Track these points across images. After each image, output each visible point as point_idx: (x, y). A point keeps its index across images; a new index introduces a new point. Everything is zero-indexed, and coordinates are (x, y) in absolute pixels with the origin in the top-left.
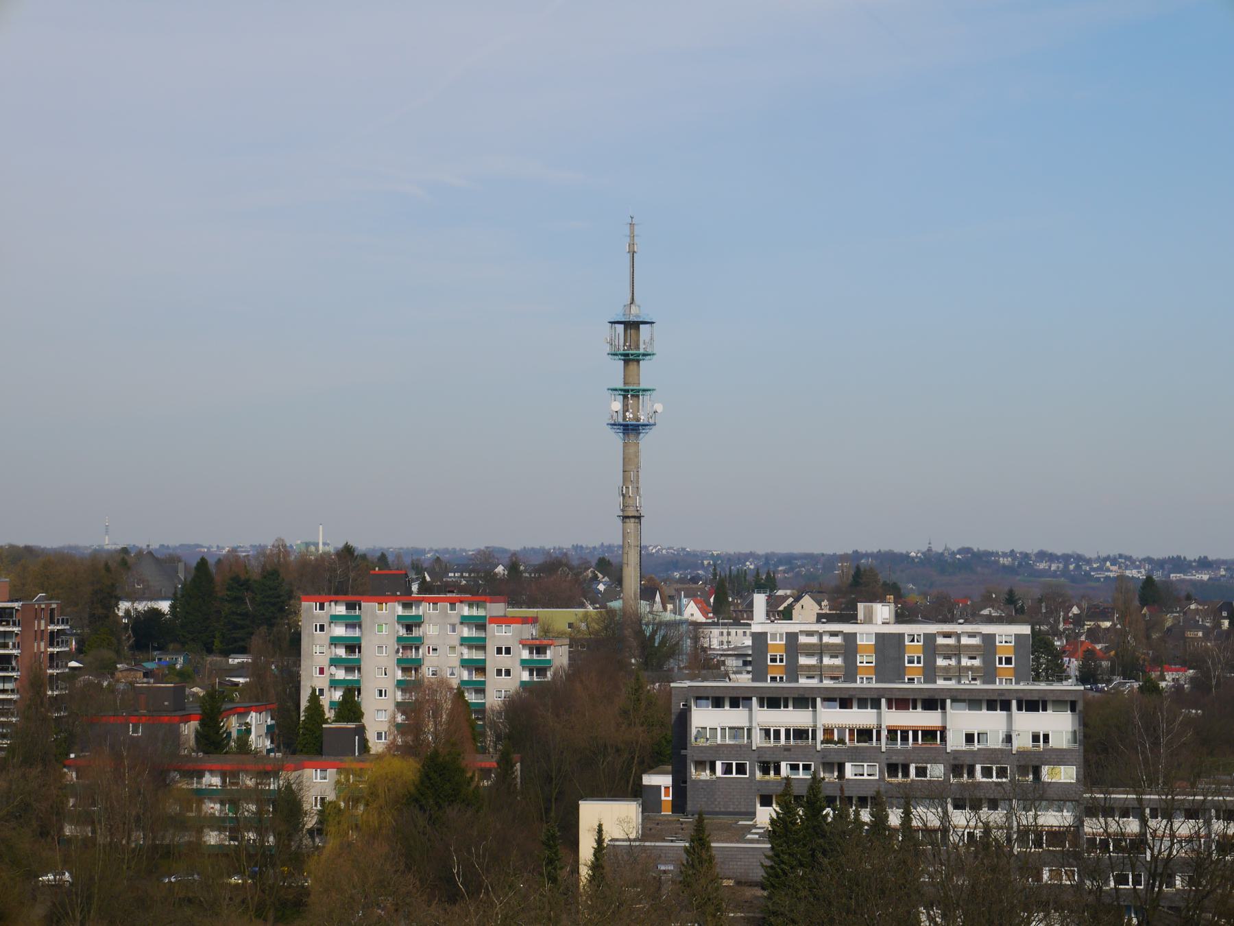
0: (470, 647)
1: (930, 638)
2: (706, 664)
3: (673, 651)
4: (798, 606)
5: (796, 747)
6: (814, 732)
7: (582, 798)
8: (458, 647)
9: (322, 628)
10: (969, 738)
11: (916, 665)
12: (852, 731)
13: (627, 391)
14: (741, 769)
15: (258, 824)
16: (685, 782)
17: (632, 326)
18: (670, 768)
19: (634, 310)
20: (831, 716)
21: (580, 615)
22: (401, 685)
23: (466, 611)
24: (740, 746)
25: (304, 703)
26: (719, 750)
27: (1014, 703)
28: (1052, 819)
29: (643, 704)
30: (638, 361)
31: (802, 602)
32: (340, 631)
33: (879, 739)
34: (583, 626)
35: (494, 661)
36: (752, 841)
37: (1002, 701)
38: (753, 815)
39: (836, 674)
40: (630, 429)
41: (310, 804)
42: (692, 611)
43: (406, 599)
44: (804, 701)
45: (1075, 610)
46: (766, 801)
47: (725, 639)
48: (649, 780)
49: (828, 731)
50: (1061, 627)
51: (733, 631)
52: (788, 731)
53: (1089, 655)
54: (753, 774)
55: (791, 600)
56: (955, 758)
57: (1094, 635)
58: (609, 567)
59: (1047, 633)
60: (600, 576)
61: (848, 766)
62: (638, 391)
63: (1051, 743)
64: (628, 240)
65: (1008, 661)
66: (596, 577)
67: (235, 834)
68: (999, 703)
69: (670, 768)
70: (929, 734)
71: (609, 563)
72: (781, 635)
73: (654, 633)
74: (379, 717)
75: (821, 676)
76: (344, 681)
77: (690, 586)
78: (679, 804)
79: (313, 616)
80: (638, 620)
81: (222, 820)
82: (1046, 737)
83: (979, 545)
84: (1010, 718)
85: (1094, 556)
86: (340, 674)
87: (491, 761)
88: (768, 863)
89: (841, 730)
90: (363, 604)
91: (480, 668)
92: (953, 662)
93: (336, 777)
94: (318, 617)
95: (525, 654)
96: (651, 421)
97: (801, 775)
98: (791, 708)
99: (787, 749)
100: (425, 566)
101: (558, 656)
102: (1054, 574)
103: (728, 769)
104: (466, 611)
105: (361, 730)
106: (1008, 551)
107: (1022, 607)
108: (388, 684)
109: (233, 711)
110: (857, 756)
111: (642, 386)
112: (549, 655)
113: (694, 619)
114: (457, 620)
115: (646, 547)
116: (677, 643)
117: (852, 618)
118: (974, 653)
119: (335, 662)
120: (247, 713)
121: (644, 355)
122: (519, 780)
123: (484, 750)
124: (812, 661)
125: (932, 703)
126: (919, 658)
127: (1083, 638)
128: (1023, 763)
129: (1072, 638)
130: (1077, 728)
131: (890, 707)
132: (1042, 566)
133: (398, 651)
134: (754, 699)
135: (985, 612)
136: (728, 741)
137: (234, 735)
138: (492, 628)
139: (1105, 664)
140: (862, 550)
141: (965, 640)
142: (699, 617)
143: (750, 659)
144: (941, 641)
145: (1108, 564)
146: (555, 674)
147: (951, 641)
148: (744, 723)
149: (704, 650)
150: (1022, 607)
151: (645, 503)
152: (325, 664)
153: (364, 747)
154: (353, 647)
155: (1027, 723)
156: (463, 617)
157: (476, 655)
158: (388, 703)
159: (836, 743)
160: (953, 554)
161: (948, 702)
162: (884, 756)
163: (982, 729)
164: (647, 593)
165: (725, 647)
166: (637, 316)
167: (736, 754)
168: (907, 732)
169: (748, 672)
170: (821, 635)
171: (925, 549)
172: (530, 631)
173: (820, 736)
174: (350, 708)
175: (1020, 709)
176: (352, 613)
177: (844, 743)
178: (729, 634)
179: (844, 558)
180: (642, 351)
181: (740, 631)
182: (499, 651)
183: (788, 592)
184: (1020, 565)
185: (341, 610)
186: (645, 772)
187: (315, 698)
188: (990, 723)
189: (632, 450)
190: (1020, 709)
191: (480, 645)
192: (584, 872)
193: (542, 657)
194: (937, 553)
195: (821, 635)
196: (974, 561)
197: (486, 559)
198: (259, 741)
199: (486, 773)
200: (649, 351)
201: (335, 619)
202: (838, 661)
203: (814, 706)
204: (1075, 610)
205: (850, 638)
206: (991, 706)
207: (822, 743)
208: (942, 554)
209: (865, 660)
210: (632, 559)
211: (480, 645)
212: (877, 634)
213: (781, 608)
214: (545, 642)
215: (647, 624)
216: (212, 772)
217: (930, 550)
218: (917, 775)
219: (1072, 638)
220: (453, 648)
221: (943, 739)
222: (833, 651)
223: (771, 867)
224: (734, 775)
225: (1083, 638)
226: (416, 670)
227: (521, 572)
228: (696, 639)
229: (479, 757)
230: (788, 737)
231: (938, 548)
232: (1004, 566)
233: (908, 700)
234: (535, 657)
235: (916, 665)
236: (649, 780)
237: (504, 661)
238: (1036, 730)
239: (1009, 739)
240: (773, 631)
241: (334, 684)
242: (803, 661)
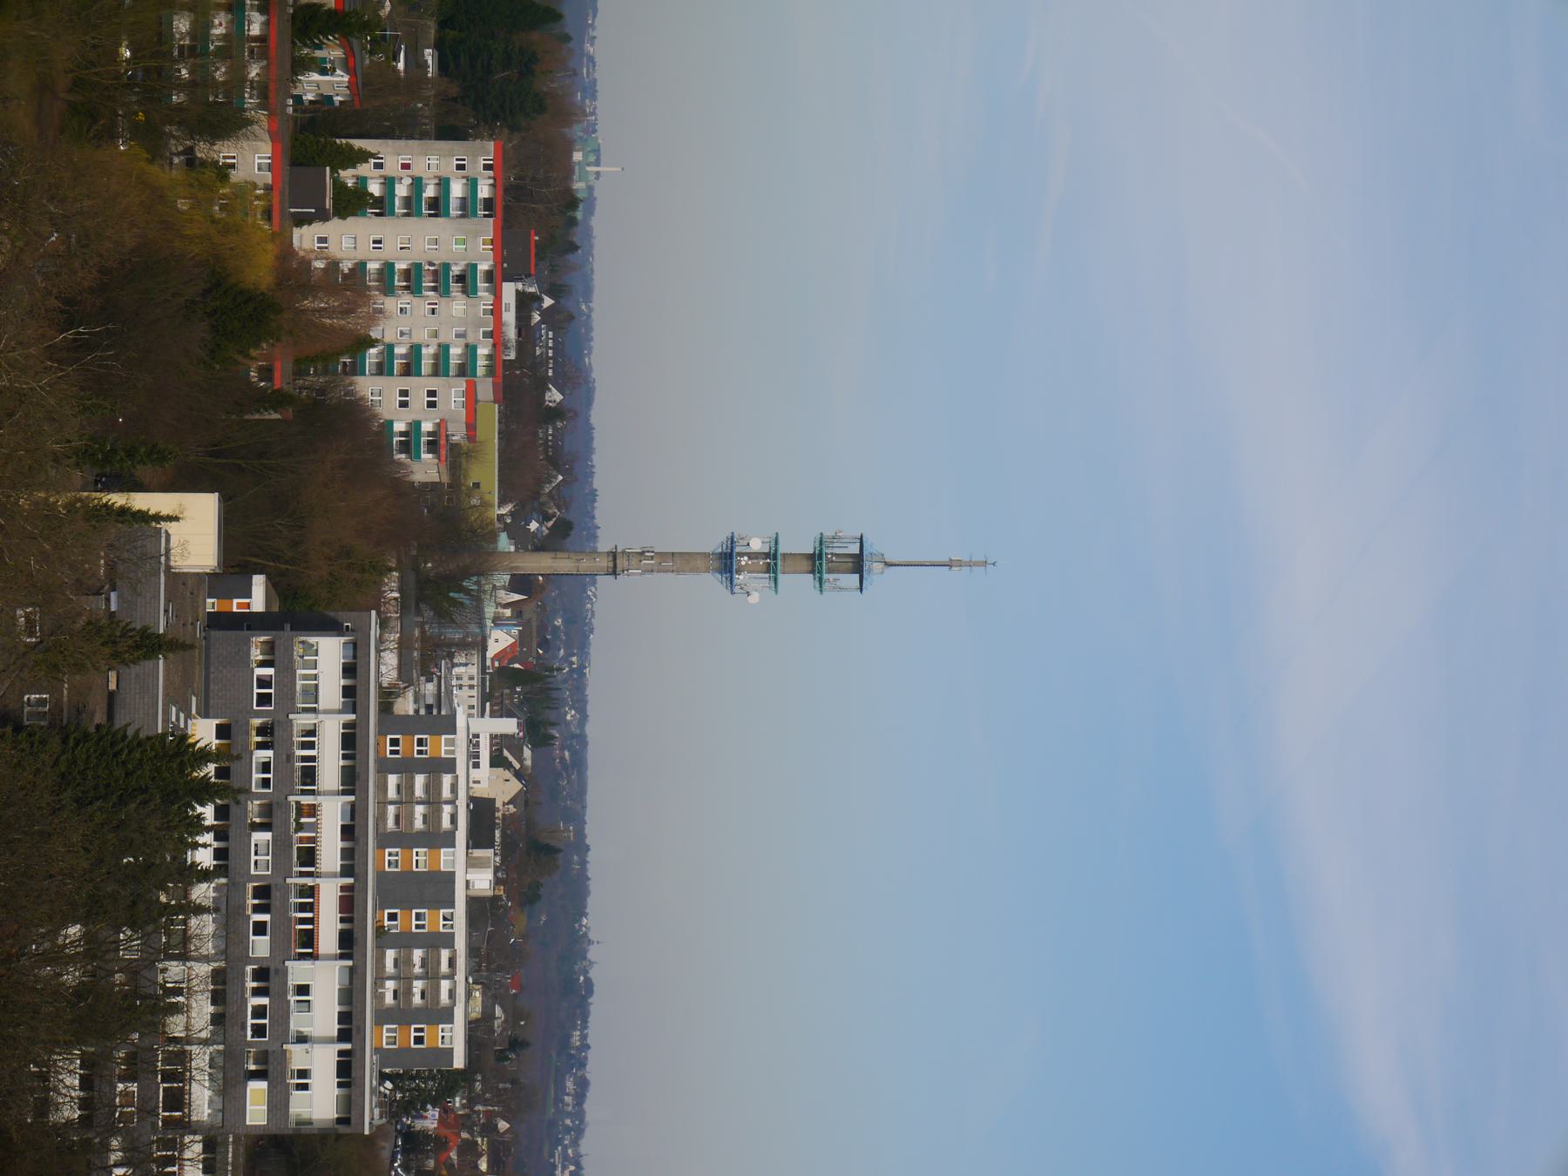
0: (436, 356)
1: (448, 940)
2: (426, 658)
3: (444, 616)
4: (507, 774)
5: (292, 770)
6: (312, 793)
7: (225, 501)
8: (435, 341)
9: (461, 167)
10: (303, 990)
11: (414, 922)
12: (313, 840)
13: (775, 558)
14: (264, 699)
15: (201, 82)
16: (249, 628)
17: (857, 564)
18: (275, 609)
19: (877, 567)
20: (332, 814)
21: (487, 497)
22: (388, 268)
23: (483, 351)
24: (293, 698)
25: (358, 143)
26: (287, 672)
27: (348, 1046)
28: (202, 1100)
29: (357, 576)
30: (812, 572)
31: (514, 780)
32: (457, 190)
33: (302, 874)
34: (474, 501)
35: (419, 387)
36: (166, 713)
37: (350, 1030)
38: (205, 713)
39: (403, 822)
40: (726, 562)
41: (224, 151)
42: (500, 641)
43: (497, 276)
44: (351, 780)
45: (503, 1125)
46: (222, 731)
47: (465, 681)
48: (259, 583)
49: (313, 811)
50: (480, 1108)
51: (474, 692)
52: (313, 759)
53: (440, 1143)
54: (258, 714)
55: (517, 766)
56: (277, 971)
57: (469, 1149)
58: (561, 536)
59: (471, 1088)
60: (550, 524)
61: (268, 836)
62: (775, 572)
63: (296, 1093)
64: (966, 559)
65: (419, 1040)
66: (547, 518)
67: (225, 53)
68: (349, 1026)
69: (275, 609)
70: (309, 939)
71: (566, 535)
72: (453, 752)
73: (467, 592)
74: (344, 241)
75: (401, 803)
76: (393, 195)
77: (536, 634)
78: (222, 621)
79: (476, 156)
80: (483, 572)
81: (206, 37)
82: (305, 1087)
83: (597, 1005)
84: (327, 1041)
85: (583, 1149)
86: (401, 190)
87: (281, 380)
88: (130, 732)
89: (314, 827)
90: (491, 220)
91: (410, 369)
92: (417, 970)
93: (260, 184)
94: (475, 162)
95: (427, 427)
96: (737, 589)
97: (257, 776)
98: (342, 763)
99: (290, 757)
100: (563, 301)
101: (426, 469)
102: (559, 1100)
103: (263, 682)
104: (483, 351)
105: (323, 216)
106: (589, 1041)
107: (507, 1059)
108: (389, 251)
109: (349, 52)
110: (280, 847)
111: (780, 576)
112: (426, 456)
113: (491, 642)
114: (471, 339)
115: (594, 583)
116: (453, 621)
117: (478, 838)
118: (428, 996)
119: (417, 184)
120: (347, 70)
121: (820, 579)
122: (257, 416)
123: (299, 372)
124: (419, 791)
125: (348, 942)
126: (423, 927)
127: (465, 1135)
128: (271, 1059)
129: (465, 1122)
130: (316, 1126)
131: (343, 888)
132: (570, 1085)
133: (431, 264)
134: (353, 717)
135: (498, 1011)
136: (299, 683)
137: (318, 54)
138: (462, 384)
139: (431, 1164)
140: (591, 856)
141: (445, 985)
142: (493, 649)
143: (435, 712)
144: (445, 954)
145: (572, 1168)
146: (400, 464)
147: (444, 967)
148: (323, 703)
149: (451, 656)
150: (507, 1059)
151: (633, 581)
152: (415, 171)
153: (301, 220)
154: (437, 207)
155: (322, 1062)
156: (474, 348)
157: (426, 364)
158: (365, 250)
159: (297, 820)
160: (585, 973)
161: (350, 963)
162: (280, 881)
163: (315, 1005)
164: (521, 583)
165: (454, 682)
166: (870, 571)
167: (285, 694)
168: (311, 910)
169: (417, 711)
170: (452, 802)
171: (591, 936)
172: (458, 434)
173: (306, 800)
174: (352, 202)
175: (341, 1053)
176: (480, 206)
177: (296, 831)
178: (471, 687)
179: (581, 835)
180: (825, 576)
181: (474, 702)
182: (432, 393)
183: (528, 763)
184: (572, 1056)
185: (484, 192)
186: (269, 578)
187: (364, 156)
188: (323, 1016)
189: (700, 563)
190: (341, 1053)
191: (439, 369)
192: (118, 499)
193: (423, 448)
194: (586, 952)
195: (452, 802)
196: (573, 996)
197: (575, 377)
198: (311, 85)
199: (266, 373)
200: (826, 586)
201: (472, 184)
202: (419, 824)
203: (344, 793)
204: (503, 1125)
205: (448, 840)
206: (344, 1018)
207: (298, 803)
208: (585, 958)
209: (420, 858)
210: (585, 565)
211: (439, 369)
212: (453, 873)
213: (506, 753)
214: (443, 453)
215: (478, 583)
216: (267, 24)
217: (590, 942)
218: (255, 923)
219: (465, 1122)
220: (435, 334)
221: (302, 957)
222: (432, 818)
223: (125, 736)
224: (256, 691)
225: (465, 1135)
226: (407, 288)
227: (554, 424)
228: (464, 646)
229: (289, 366)
230: (304, 759)
231: (593, 953)
232: (569, 1036)
233: (351, 911)
234: (424, 439)
235: (414, 922)
236: (259, 583)
237: (419, 399)
238: (313, 1074)
239: (302, 1039)
240: (458, 742)
241: (389, 183)
242: (420, 780)
